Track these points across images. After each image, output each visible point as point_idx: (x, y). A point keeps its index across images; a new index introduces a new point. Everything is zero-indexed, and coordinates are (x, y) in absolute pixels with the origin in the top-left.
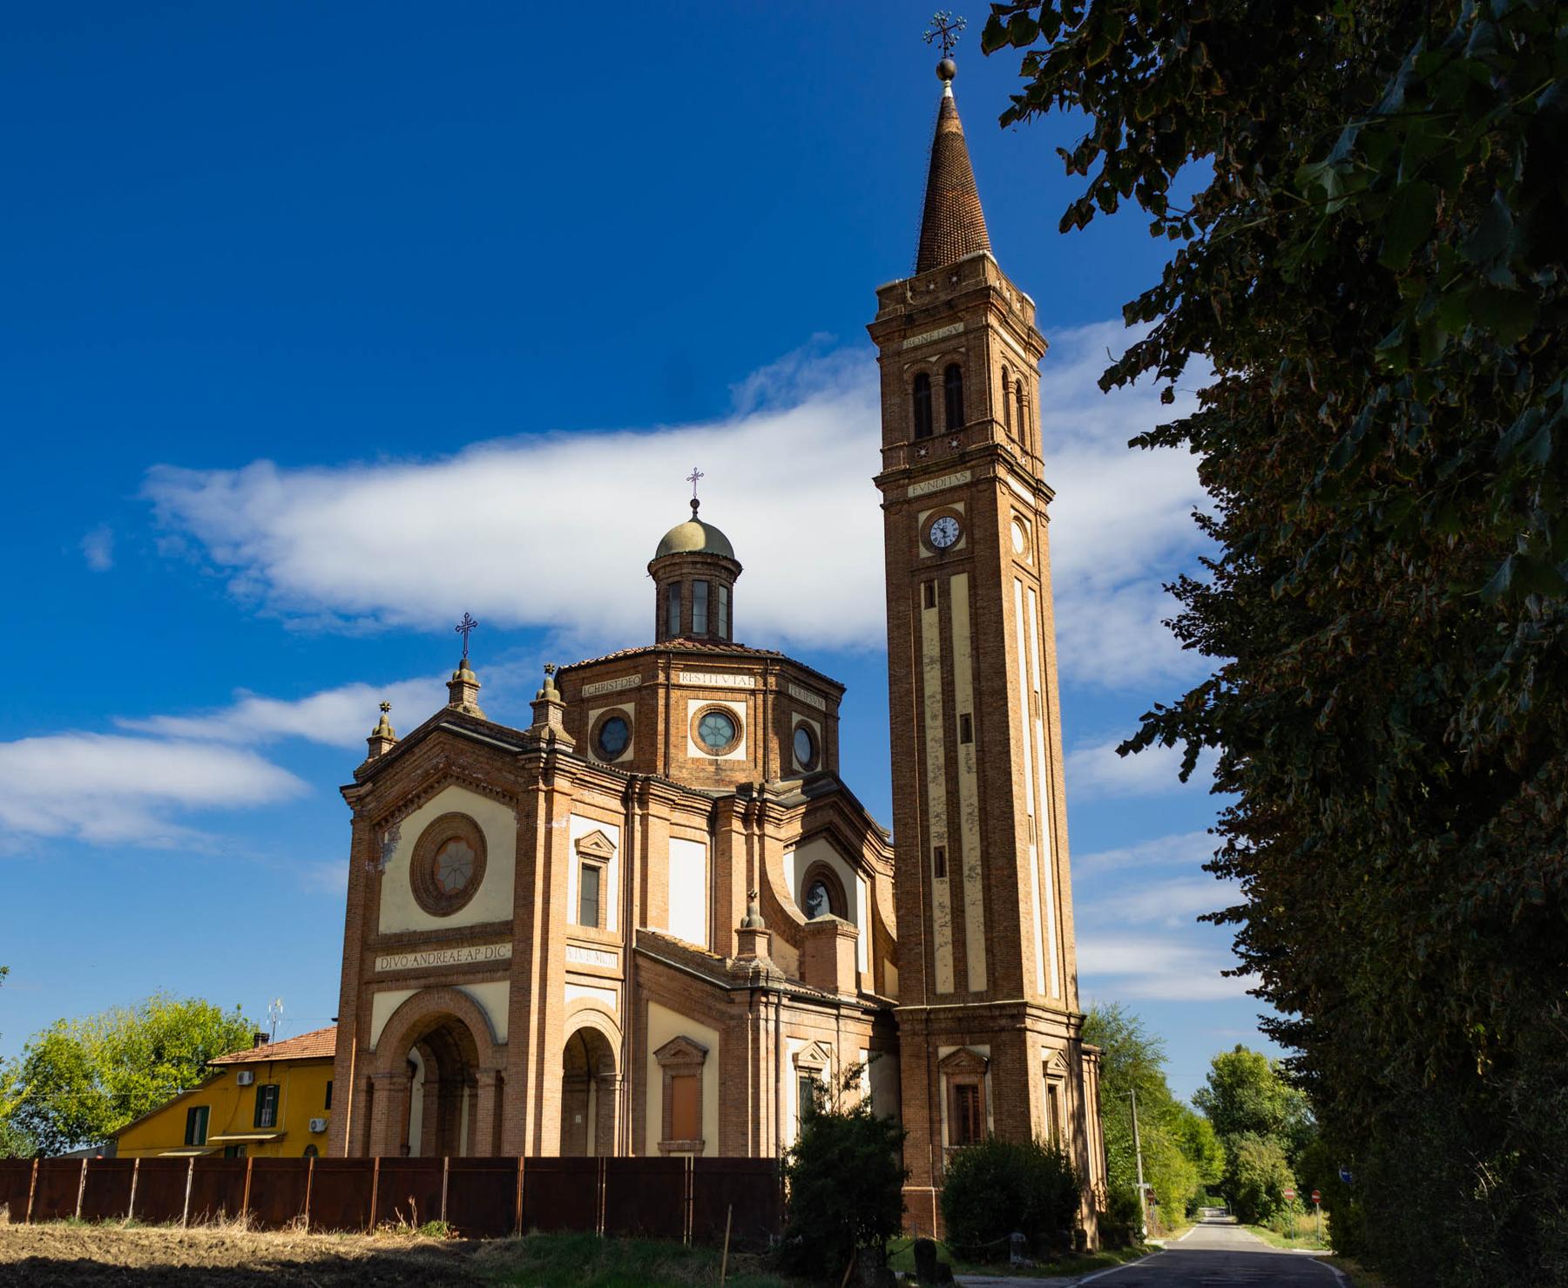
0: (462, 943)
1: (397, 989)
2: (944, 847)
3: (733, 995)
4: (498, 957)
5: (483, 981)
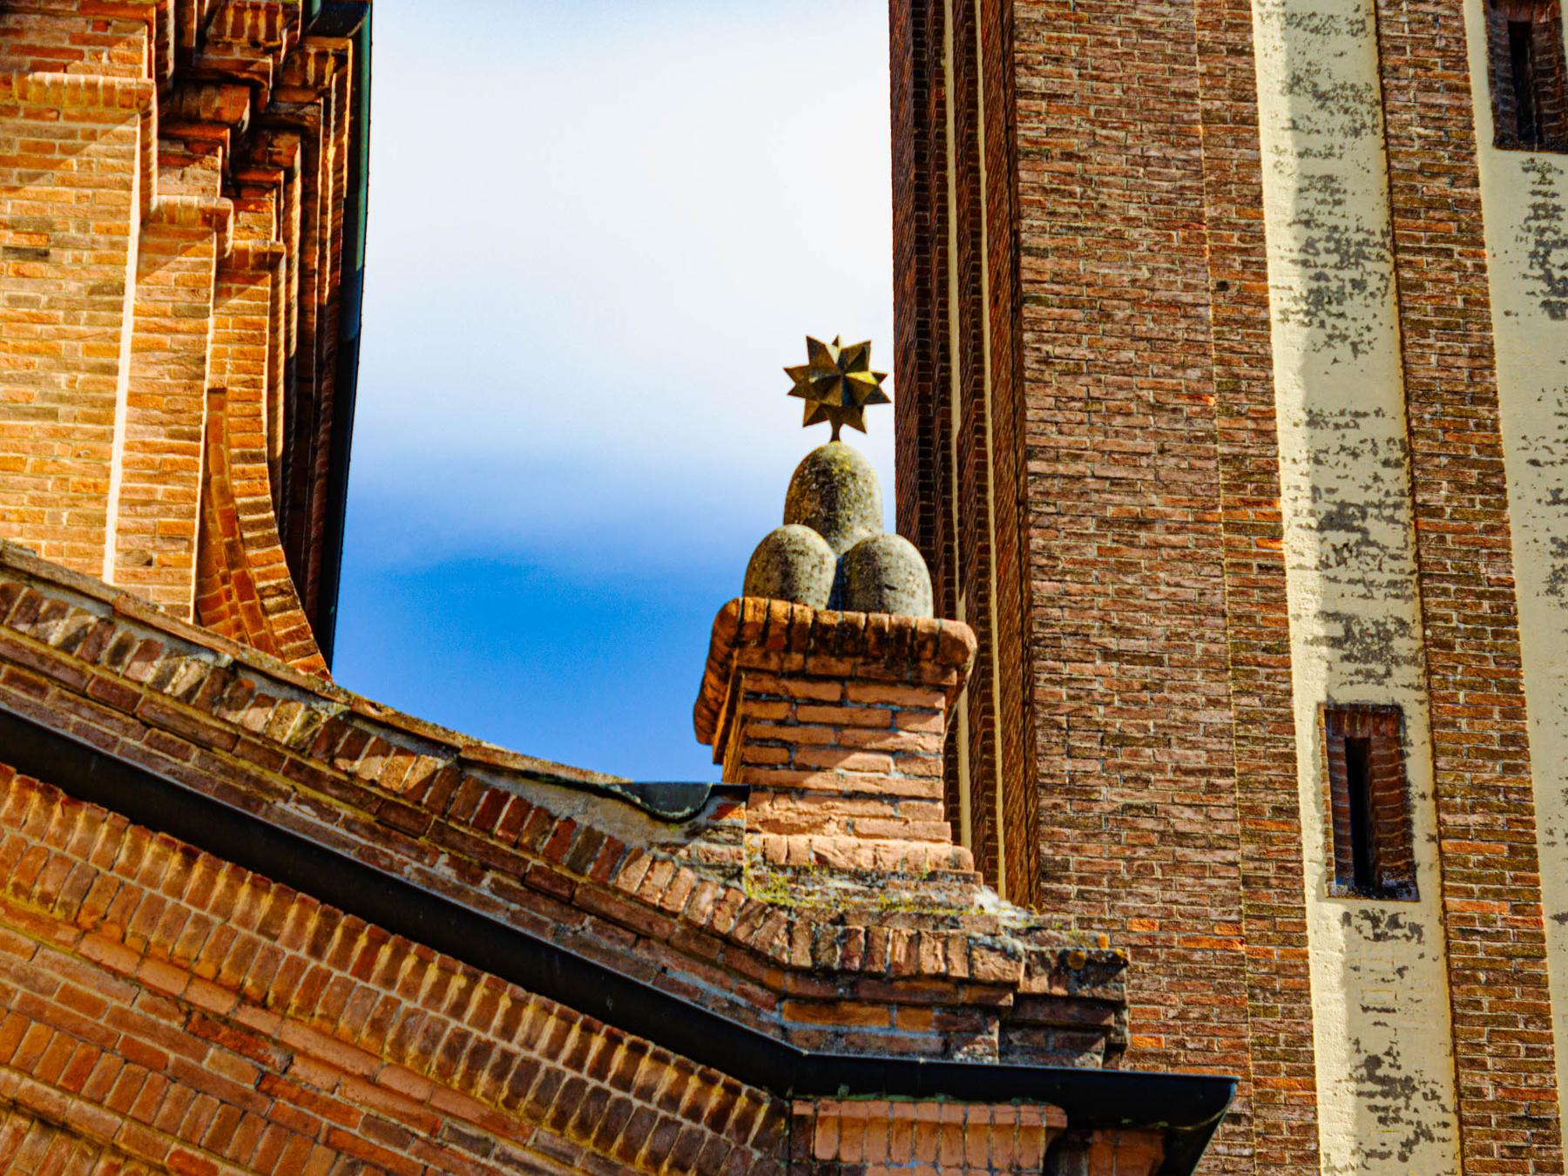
2: (1394, 714)
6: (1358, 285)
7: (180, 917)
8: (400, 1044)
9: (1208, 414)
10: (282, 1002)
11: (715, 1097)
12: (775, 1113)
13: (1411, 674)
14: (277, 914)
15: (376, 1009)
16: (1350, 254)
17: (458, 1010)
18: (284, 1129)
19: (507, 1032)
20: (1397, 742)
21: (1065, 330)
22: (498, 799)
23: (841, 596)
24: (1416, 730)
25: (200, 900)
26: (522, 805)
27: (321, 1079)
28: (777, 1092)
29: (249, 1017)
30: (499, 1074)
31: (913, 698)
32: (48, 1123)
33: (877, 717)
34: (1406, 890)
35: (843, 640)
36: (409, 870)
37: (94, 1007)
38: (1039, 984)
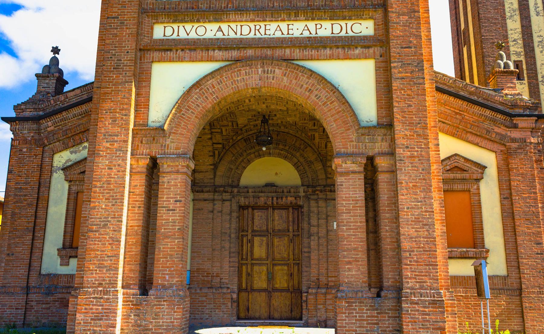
0: (296, 15)
1: (192, 60)
2: (521, 61)
3: (516, 120)
4: (350, 34)
5: (331, 58)
6: (515, 14)
7: (454, 104)
8: (475, 114)
9: (500, 30)
10: (464, 111)
11: (504, 118)
12: (510, 119)
13: (523, 57)
14: (463, 103)
15: (473, 111)
16: (514, 11)
17: (480, 111)
18: (465, 122)
19: (485, 113)
20: (522, 64)
21: (485, 23)
22: (481, 91)
23: (504, 68)
24: (524, 63)
25: (456, 102)
26: (483, 91)
27: (468, 118)
28: (510, 117)
29: (461, 112)
30: (484, 117)
31: (513, 77)
32: (444, 123)
33: (510, 79)
34: (523, 80)
35: (504, 72)
36: (473, 98)
37: (447, 112)
38: (531, 105)
